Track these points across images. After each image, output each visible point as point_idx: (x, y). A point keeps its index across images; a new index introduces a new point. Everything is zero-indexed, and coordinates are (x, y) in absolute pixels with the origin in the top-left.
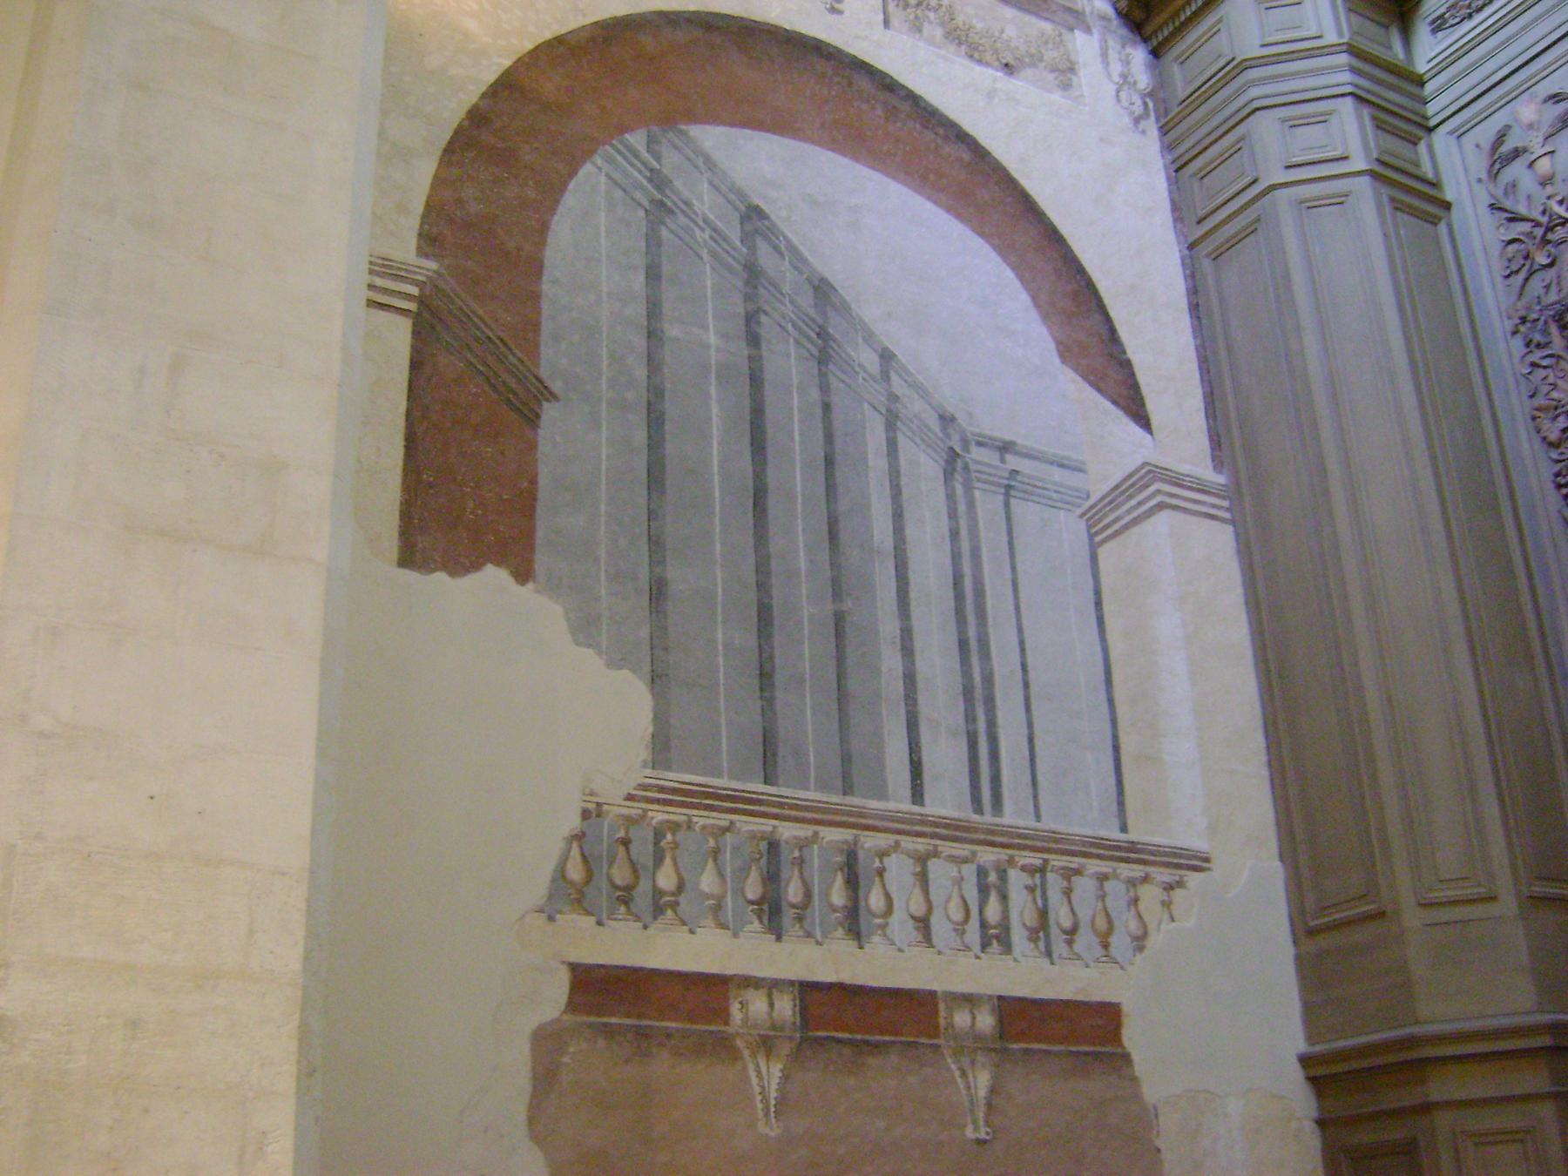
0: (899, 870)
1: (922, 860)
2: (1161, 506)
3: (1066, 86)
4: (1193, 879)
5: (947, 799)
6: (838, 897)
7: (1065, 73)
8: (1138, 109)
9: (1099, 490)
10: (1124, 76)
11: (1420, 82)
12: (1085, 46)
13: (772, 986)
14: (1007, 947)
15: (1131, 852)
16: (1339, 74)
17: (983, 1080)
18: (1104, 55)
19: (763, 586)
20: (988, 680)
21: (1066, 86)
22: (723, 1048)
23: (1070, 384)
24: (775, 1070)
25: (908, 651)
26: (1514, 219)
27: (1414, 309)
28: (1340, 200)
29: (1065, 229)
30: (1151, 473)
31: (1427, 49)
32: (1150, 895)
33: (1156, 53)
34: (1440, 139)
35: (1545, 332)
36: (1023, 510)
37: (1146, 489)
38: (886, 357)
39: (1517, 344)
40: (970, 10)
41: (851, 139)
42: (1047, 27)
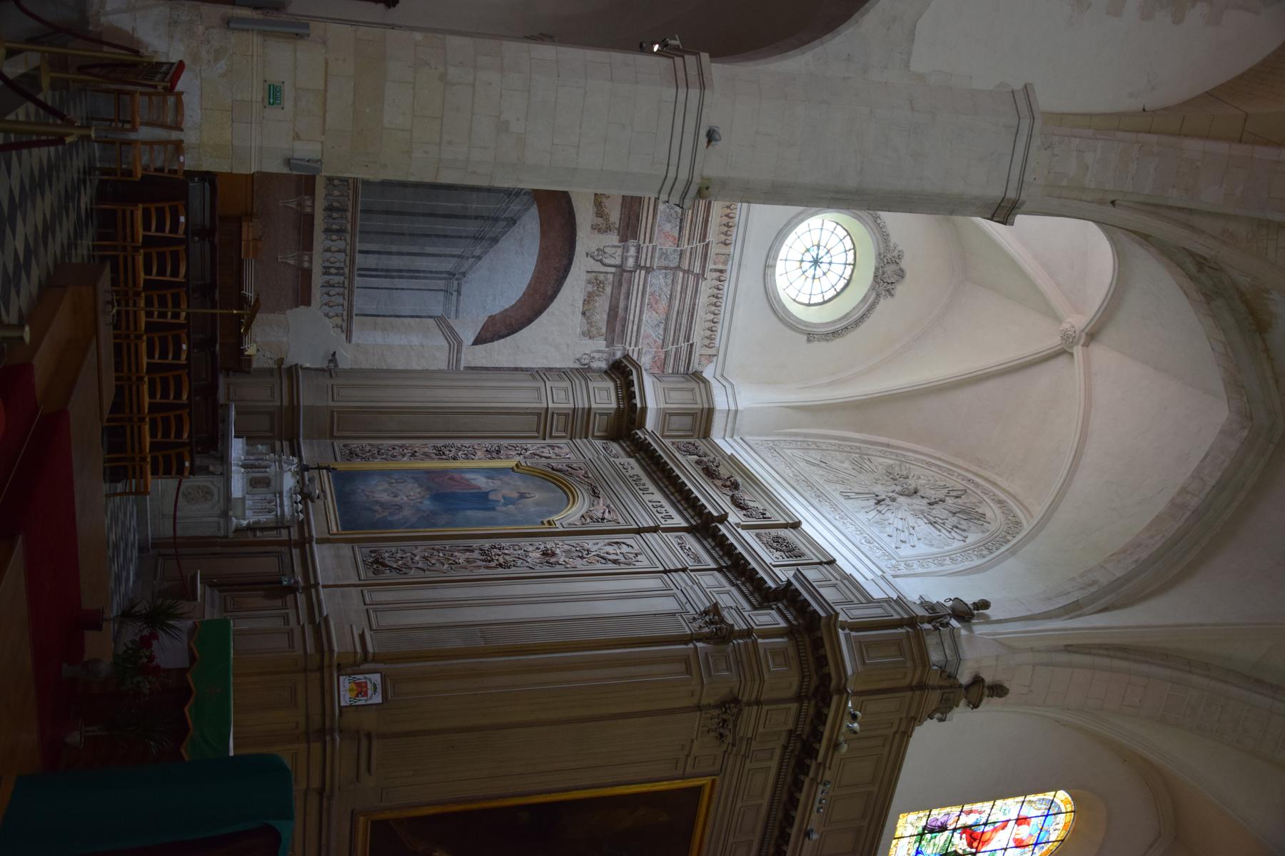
0: (341, 244)
1: (344, 251)
4: (344, 336)
5: (360, 260)
6: (334, 227)
9: (452, 322)
13: (313, 207)
14: (325, 274)
15: (350, 317)
17: (292, 262)
19: (409, 214)
20: (392, 277)
24: (293, 206)
25: (398, 254)
29: (533, 325)
30: (460, 343)
33: (606, 372)
38: (479, 258)
41: (543, 257)
42: (604, 330)
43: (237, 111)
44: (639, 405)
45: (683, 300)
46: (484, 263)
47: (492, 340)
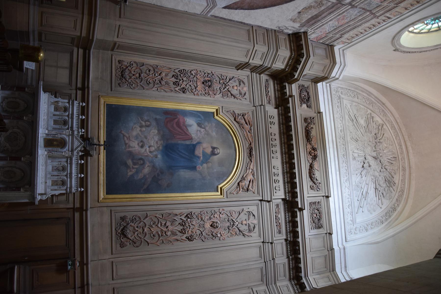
2: (208, 5)
3: (291, 20)
7: (294, 21)
8: (281, 28)
10: (288, 29)
11: (260, 74)
12: (297, 25)
16: (267, 64)
18: (293, 27)
21: (291, 20)
26: (230, 80)
27: (232, 39)
28: (246, 56)
30: (215, 5)
31: (264, 77)
33: (289, 35)
34: (249, 73)
35: (209, 77)
39: (210, 72)
40: (313, 11)
42: (304, 21)
43: (27, 18)
44: (296, 77)
45: (358, 22)
47: (236, 9)
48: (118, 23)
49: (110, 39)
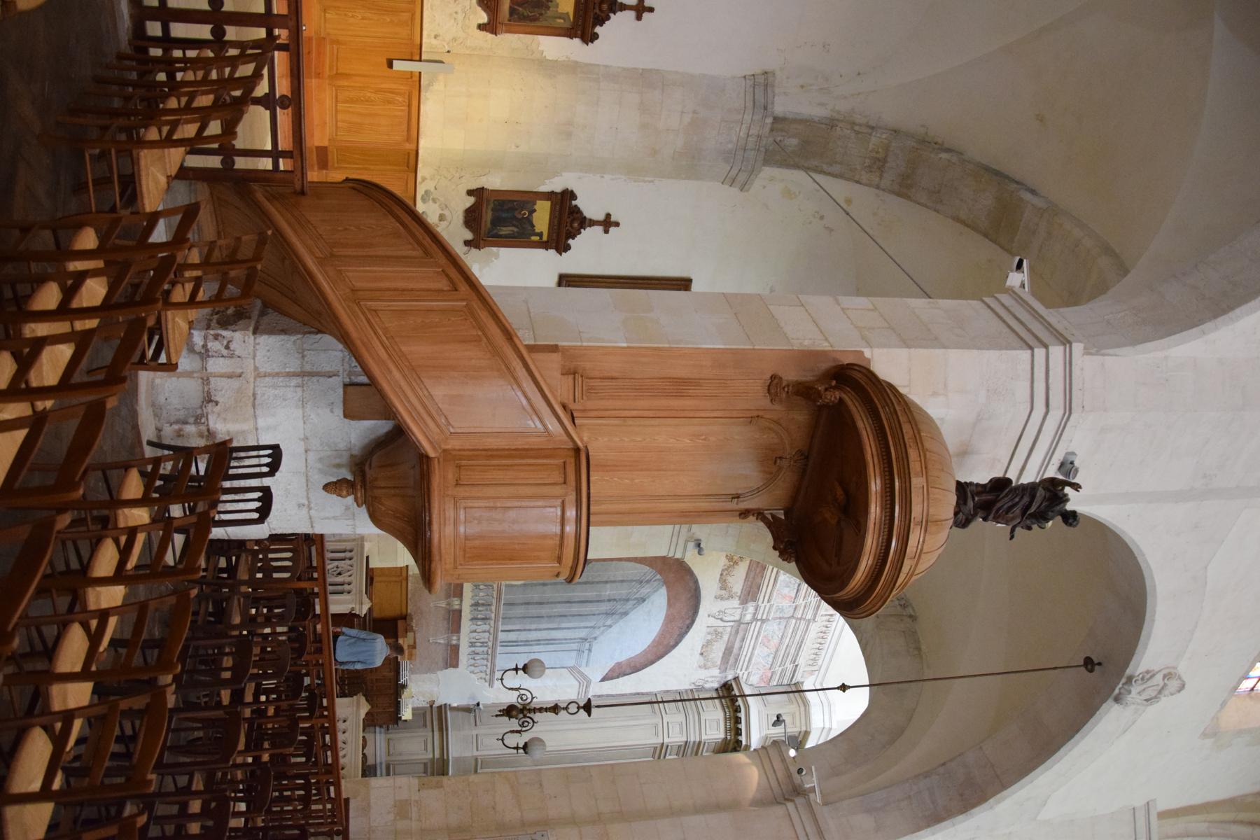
0: (486, 627)
5: (502, 636)
9: (582, 670)
16: (694, 738)
22: (448, 596)
23: (611, 664)
28: (426, 749)
30: (589, 682)
32: (483, 675)
36: (574, 654)
37: (585, 681)
38: (610, 626)
46: (615, 629)
48: (474, 733)
49: (468, 754)
